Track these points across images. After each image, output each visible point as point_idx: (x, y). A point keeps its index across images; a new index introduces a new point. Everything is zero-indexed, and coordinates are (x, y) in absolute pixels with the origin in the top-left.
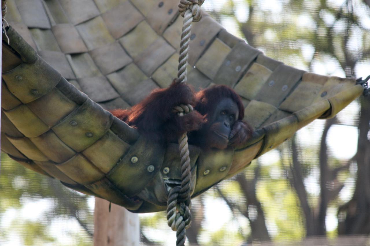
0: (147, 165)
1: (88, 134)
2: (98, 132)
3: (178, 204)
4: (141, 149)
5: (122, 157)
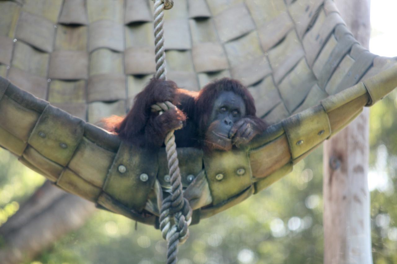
0: (138, 173)
1: (62, 146)
2: (70, 141)
3: (171, 215)
4: (125, 157)
5: (109, 167)
